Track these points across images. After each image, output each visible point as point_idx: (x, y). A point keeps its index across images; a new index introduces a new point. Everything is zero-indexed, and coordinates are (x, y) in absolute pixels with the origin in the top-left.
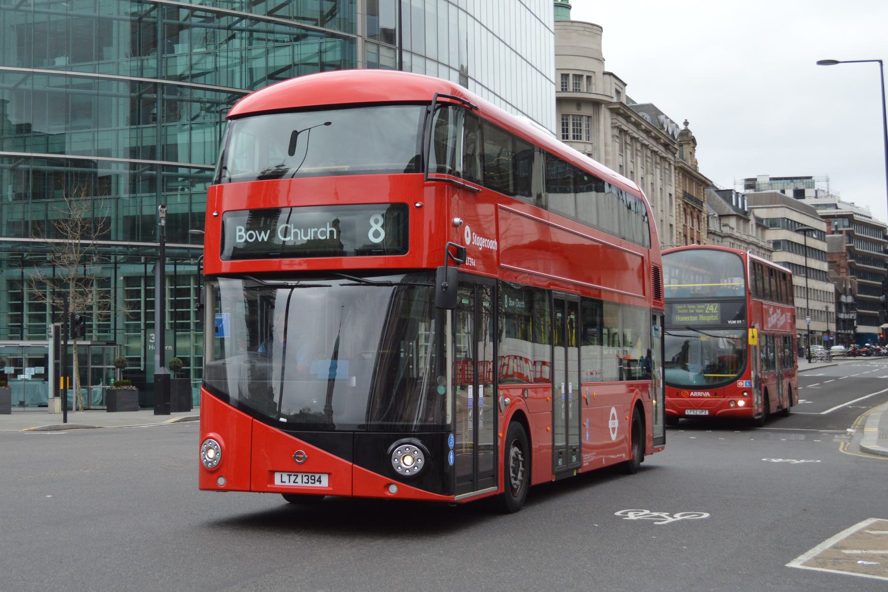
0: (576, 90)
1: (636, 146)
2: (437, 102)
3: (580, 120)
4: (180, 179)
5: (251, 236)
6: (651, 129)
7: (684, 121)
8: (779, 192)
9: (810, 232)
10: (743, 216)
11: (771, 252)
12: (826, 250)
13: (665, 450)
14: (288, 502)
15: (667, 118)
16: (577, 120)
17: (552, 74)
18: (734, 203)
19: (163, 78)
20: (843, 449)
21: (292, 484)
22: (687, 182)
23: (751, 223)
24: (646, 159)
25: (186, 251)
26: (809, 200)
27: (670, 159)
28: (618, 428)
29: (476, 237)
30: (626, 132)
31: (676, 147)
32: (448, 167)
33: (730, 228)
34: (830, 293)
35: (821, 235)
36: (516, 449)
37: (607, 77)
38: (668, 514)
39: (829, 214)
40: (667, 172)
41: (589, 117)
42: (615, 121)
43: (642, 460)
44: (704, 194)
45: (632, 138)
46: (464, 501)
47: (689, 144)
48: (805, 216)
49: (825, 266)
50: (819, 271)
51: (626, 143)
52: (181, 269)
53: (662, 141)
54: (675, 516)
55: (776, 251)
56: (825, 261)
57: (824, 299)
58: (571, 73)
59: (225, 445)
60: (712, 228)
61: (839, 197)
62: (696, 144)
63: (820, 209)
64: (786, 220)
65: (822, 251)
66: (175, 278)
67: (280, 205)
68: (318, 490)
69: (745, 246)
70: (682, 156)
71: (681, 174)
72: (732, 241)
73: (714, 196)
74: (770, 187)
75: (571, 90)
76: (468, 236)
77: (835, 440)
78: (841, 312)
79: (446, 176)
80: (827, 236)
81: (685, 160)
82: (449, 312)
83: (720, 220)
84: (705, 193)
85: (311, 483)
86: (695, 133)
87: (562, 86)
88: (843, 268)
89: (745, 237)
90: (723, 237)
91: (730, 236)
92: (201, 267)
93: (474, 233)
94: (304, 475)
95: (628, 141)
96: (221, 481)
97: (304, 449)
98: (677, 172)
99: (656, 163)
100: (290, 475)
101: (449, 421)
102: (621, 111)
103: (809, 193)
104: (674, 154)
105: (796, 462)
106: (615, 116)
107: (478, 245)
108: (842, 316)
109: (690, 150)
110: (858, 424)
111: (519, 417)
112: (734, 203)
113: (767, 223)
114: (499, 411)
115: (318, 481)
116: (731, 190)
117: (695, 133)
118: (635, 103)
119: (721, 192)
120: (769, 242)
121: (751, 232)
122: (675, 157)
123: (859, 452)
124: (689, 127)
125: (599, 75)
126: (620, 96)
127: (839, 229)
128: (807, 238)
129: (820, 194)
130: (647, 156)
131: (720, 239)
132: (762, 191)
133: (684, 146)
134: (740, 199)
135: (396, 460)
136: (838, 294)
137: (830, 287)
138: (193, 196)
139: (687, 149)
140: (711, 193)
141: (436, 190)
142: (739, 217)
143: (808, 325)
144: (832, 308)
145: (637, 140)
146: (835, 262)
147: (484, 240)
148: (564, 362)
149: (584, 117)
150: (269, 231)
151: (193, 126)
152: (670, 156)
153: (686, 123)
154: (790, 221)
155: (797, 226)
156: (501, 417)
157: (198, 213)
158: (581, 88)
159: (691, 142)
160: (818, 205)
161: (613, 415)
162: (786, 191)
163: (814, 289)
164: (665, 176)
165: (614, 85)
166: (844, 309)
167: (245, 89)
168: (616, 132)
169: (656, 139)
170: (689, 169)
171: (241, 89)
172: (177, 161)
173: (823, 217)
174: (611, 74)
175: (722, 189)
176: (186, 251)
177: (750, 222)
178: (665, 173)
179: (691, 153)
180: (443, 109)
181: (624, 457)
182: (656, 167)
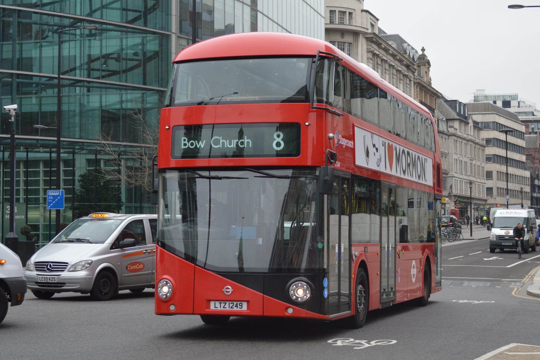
0: (341, 22)
1: (385, 66)
2: (320, 56)
3: (344, 46)
4: (34, 85)
5: (192, 144)
6: (397, 54)
7: (422, 48)
8: (491, 102)
9: (511, 133)
10: (464, 120)
11: (485, 147)
12: (524, 146)
13: (442, 289)
14: (204, 323)
15: (409, 45)
16: (341, 46)
17: (322, 10)
18: (458, 111)
19: (18, 6)
20: (515, 293)
21: (222, 308)
22: (423, 94)
23: (470, 125)
24: (393, 76)
25: (35, 142)
26: (512, 110)
27: (410, 76)
28: (416, 274)
30: (377, 56)
31: (415, 67)
32: (325, 99)
33: (454, 129)
34: (527, 178)
35: (520, 135)
36: (361, 286)
37: (364, 13)
38: (366, 341)
39: (528, 119)
40: (408, 86)
41: (350, 44)
42: (369, 47)
43: (429, 296)
44: (435, 103)
45: (382, 60)
47: (425, 65)
48: (510, 121)
49: (523, 158)
50: (519, 161)
51: (377, 64)
52: (31, 155)
53: (405, 63)
54: (371, 343)
55: (488, 147)
56: (524, 154)
57: (522, 182)
58: (337, 10)
59: (176, 284)
60: (441, 129)
61: (535, 107)
62: (430, 66)
63: (522, 116)
64: (496, 123)
65: (521, 147)
66: (28, 163)
67: (204, 122)
68: (241, 312)
69: (465, 142)
70: (419, 75)
71: (418, 88)
72: (456, 139)
73: (443, 105)
74: (485, 99)
75: (337, 23)
77: (511, 286)
78: (535, 192)
79: (324, 105)
80: (525, 136)
81: (421, 78)
82: (326, 196)
83: (447, 123)
84: (437, 102)
85: (240, 308)
86: (429, 58)
87: (330, 20)
88: (537, 159)
89: (465, 136)
90: (449, 136)
91: (454, 135)
92: (155, 163)
94: (230, 302)
95: (379, 62)
96: (172, 308)
98: (415, 86)
99: (400, 79)
100: (220, 303)
101: (325, 267)
102: (374, 40)
103: (514, 103)
104: (413, 73)
105: (476, 302)
106: (370, 44)
107: (343, 144)
108: (535, 195)
109: (426, 70)
110: (532, 274)
111: (363, 265)
112: (458, 111)
113: (482, 125)
115: (235, 306)
116: (456, 100)
117: (430, 56)
118: (386, 33)
119: (449, 102)
120: (483, 139)
121: (470, 132)
122: (414, 75)
123: (527, 296)
124: (425, 53)
125: (358, 12)
126: (374, 28)
127: (535, 131)
128: (507, 135)
129: (521, 104)
130: (393, 74)
131: (447, 137)
132: (480, 101)
133: (421, 67)
134: (462, 107)
135: (292, 292)
136: (532, 179)
137: (527, 174)
138: (43, 99)
139: (423, 69)
140: (441, 102)
141: (317, 115)
142: (461, 121)
143: (508, 202)
144: (527, 189)
145: (386, 61)
146: (531, 155)
148: (337, 227)
149: (347, 43)
150: (204, 141)
151: (43, 44)
152: (411, 74)
153: (423, 50)
154: (498, 124)
155: (503, 128)
156: (353, 265)
157: (50, 112)
158: (344, 22)
159: (427, 64)
160: (520, 113)
162: (497, 102)
163: (515, 175)
164: (407, 89)
165: (369, 19)
166: (537, 190)
167: (84, 16)
168: (370, 55)
169: (400, 61)
170: (425, 84)
171: (81, 15)
172: (31, 71)
173: (523, 121)
174: (367, 11)
175: (449, 99)
176: (35, 142)
177: (469, 124)
178: (406, 87)
179: (426, 72)
180: (321, 60)
182: (400, 83)
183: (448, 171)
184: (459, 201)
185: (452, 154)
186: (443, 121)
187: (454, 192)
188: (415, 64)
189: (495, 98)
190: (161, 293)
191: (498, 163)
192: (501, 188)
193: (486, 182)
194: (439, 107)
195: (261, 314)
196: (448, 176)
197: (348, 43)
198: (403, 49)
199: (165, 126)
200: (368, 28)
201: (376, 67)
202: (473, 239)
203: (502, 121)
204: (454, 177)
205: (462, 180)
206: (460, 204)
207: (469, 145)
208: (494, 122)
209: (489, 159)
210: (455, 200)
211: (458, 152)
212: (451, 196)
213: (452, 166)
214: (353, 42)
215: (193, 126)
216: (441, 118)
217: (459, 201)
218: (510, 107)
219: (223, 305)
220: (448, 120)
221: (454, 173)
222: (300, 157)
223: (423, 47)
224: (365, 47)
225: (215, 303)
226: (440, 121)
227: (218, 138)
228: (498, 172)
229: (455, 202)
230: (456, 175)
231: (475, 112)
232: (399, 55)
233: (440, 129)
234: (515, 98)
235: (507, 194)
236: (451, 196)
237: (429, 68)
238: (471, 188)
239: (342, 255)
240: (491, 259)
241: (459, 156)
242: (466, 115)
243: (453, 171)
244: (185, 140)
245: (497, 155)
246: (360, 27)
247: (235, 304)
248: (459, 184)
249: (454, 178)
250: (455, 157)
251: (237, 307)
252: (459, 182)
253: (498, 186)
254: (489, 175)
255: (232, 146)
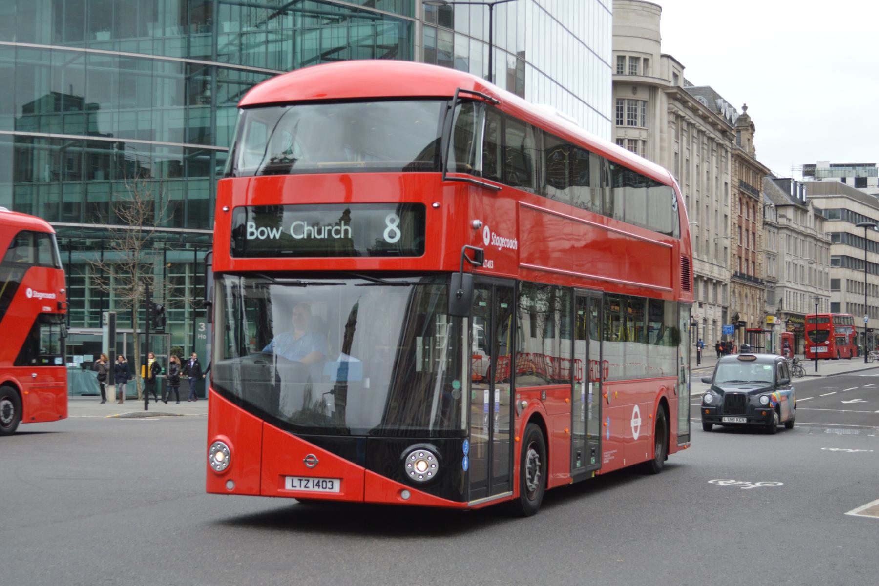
0: (632, 73)
2: (458, 97)
3: (636, 105)
5: (262, 233)
6: (708, 115)
7: (743, 105)
8: (839, 180)
10: (801, 206)
11: (830, 245)
15: (725, 101)
16: (632, 105)
17: (610, 58)
18: (792, 193)
21: (303, 489)
22: (744, 170)
23: (809, 214)
25: (177, 236)
27: (727, 146)
29: (495, 237)
33: (787, 219)
37: (665, 59)
40: (724, 160)
41: (645, 102)
42: (671, 106)
44: (761, 183)
46: (478, 507)
47: (747, 130)
48: (866, 208)
51: (682, 129)
53: (719, 127)
55: (834, 244)
58: (627, 55)
60: (768, 219)
69: (802, 238)
70: (739, 143)
71: (737, 162)
72: (788, 233)
74: (830, 174)
76: (487, 237)
81: (742, 147)
83: (777, 210)
84: (762, 182)
89: (802, 229)
90: (779, 229)
91: (786, 228)
93: (493, 234)
96: (230, 485)
97: (314, 455)
98: (733, 159)
99: (713, 150)
100: (301, 480)
101: (464, 427)
102: (679, 96)
104: (731, 141)
105: (851, 451)
106: (672, 101)
107: (497, 245)
112: (792, 193)
113: (826, 213)
114: (516, 415)
115: (316, 485)
116: (790, 179)
117: (754, 116)
119: (778, 181)
120: (827, 234)
121: (809, 223)
122: (732, 144)
124: (748, 112)
125: (657, 58)
126: (678, 79)
130: (703, 143)
131: (776, 231)
133: (742, 132)
134: (798, 188)
135: (410, 465)
139: (744, 135)
142: (796, 208)
143: (866, 324)
147: (504, 240)
152: (727, 143)
153: (745, 108)
155: (864, 220)
158: (637, 71)
159: (749, 128)
161: (636, 413)
162: (848, 179)
164: (721, 164)
168: (672, 118)
169: (714, 125)
170: (747, 157)
174: (669, 57)
175: (779, 177)
176: (177, 236)
179: (749, 139)
181: (647, 456)
182: (712, 155)
183: (777, 278)
184: (792, 322)
185: (783, 255)
186: (771, 207)
187: (786, 308)
188: (733, 128)
189: (845, 174)
190: (213, 461)
191: (848, 267)
192: (852, 304)
193: (831, 294)
194: (765, 189)
195: (360, 499)
196: (777, 285)
197: (641, 100)
198: (716, 107)
199: (223, 206)
200: (670, 80)
201: (680, 133)
202: (820, 376)
203: (856, 207)
204: (786, 287)
205: (796, 291)
206: (792, 325)
207: (808, 242)
208: (843, 210)
209: (835, 262)
210: (786, 320)
211: (792, 252)
212: (780, 314)
213: (783, 272)
214: (648, 100)
215: (267, 207)
216: (769, 204)
217: (792, 322)
218: (866, 186)
219: (304, 483)
220: (778, 207)
221: (785, 282)
222: (424, 257)
223: (745, 104)
224: (665, 106)
225: (292, 480)
226: (766, 208)
227: (302, 223)
228: (848, 280)
229: (787, 323)
230: (788, 285)
231: (816, 194)
232: (712, 117)
233: (767, 220)
234: (873, 174)
235: (866, 313)
236: (780, 314)
237: (752, 134)
238: (816, 305)
239: (590, 397)
240: (851, 401)
241: (793, 257)
242: (804, 199)
243: (783, 279)
244: (251, 227)
245: (848, 257)
246: (659, 79)
247: (316, 482)
248: (792, 297)
249: (786, 289)
250: (787, 258)
251: (319, 486)
252: (792, 294)
253: (848, 300)
254: (835, 284)
255: (322, 236)
